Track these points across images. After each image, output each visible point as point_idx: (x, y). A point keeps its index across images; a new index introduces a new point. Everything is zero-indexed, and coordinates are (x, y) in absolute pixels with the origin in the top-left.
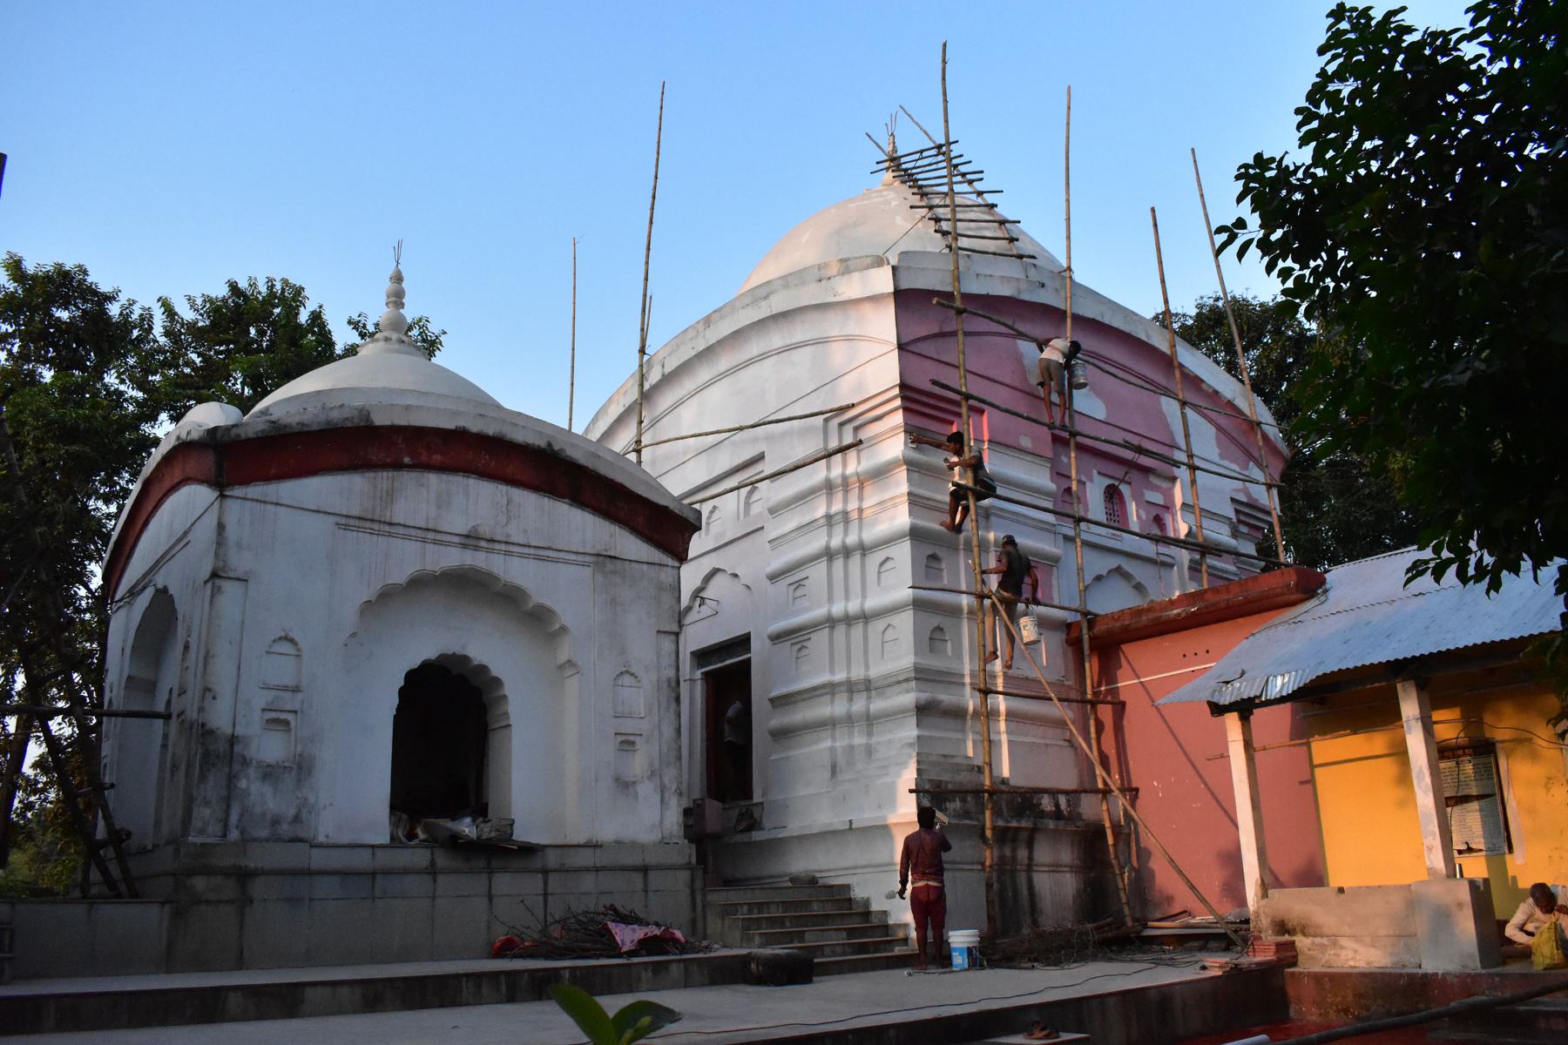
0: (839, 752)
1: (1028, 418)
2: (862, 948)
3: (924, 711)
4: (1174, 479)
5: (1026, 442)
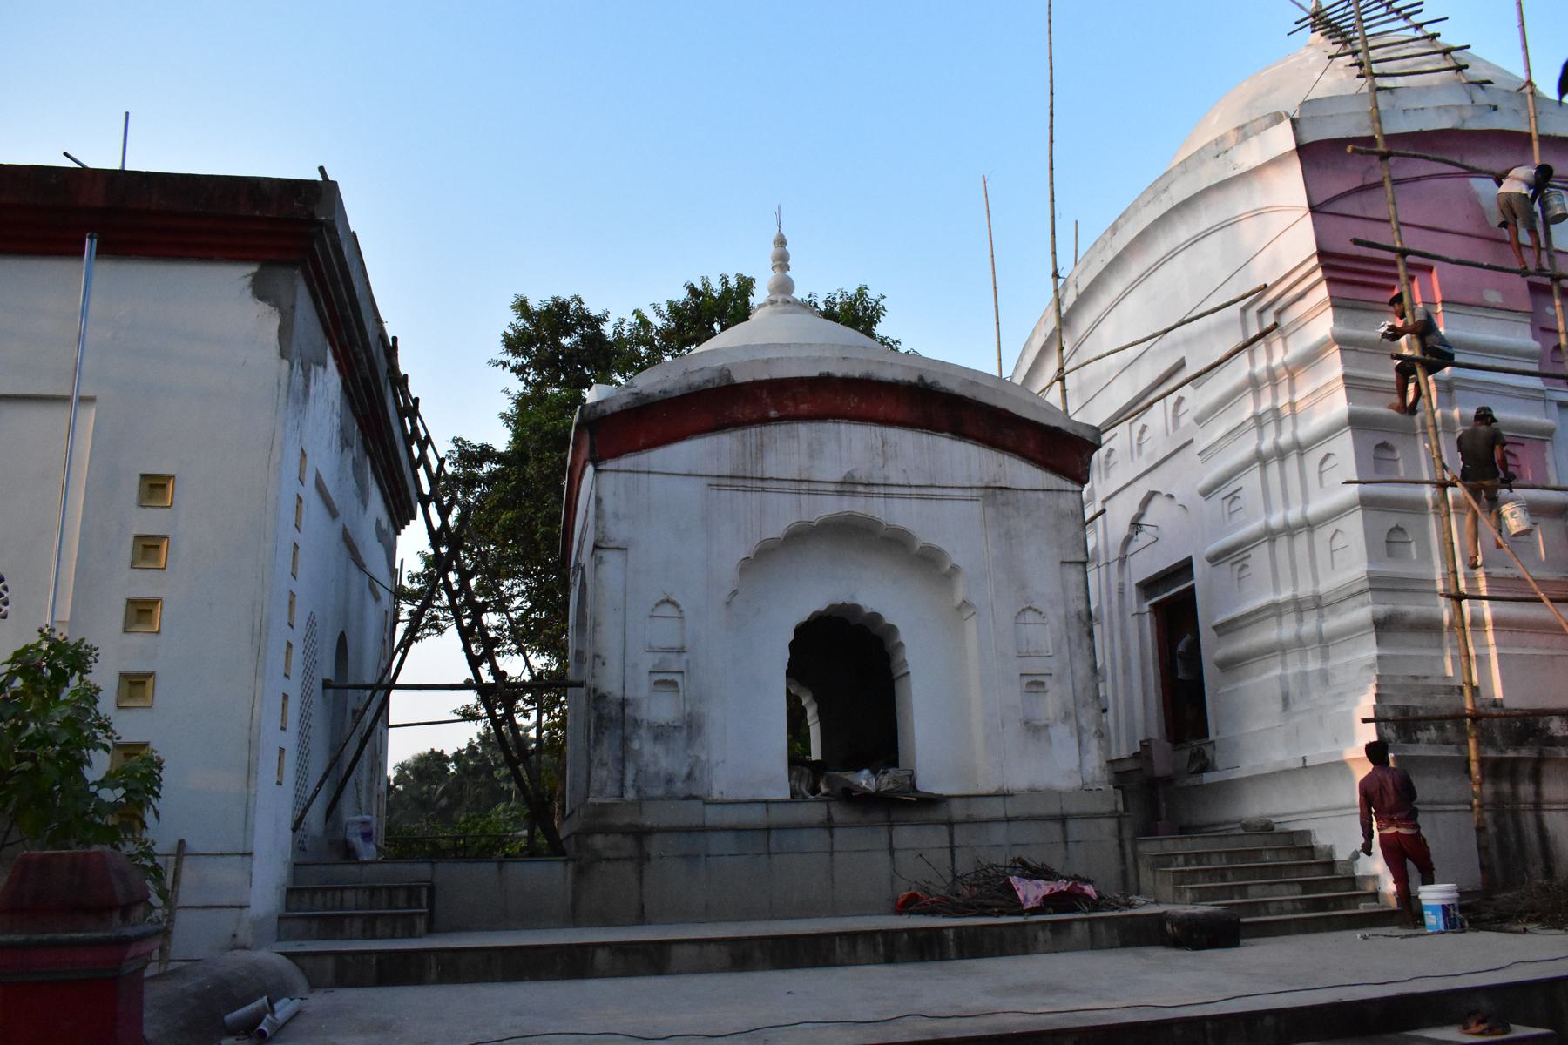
0: (1290, 680)
1: (1489, 267)
2: (1319, 904)
3: (1384, 626)
5: (1493, 297)
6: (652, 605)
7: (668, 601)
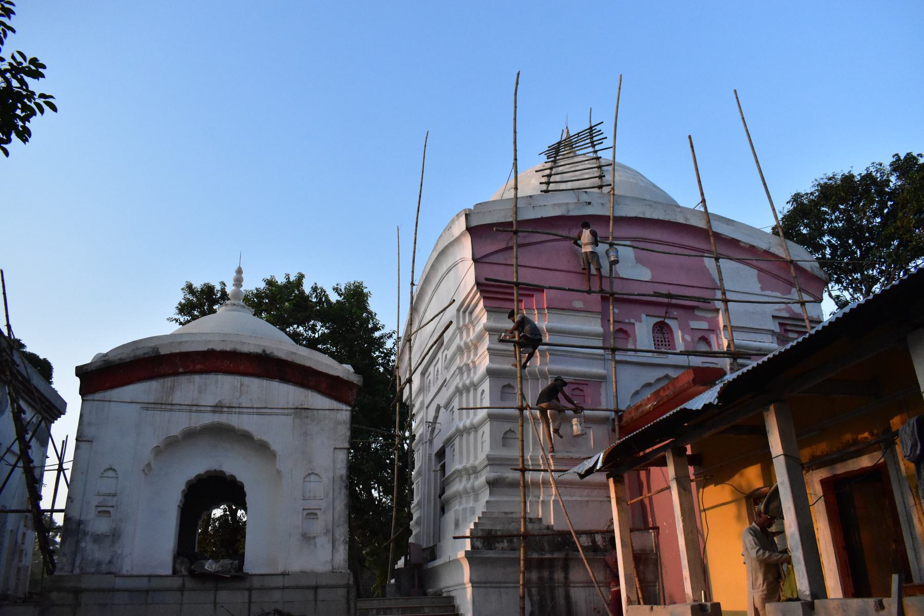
3: (493, 484)
4: (717, 310)
5: (578, 305)
6: (102, 471)
7: (111, 469)
